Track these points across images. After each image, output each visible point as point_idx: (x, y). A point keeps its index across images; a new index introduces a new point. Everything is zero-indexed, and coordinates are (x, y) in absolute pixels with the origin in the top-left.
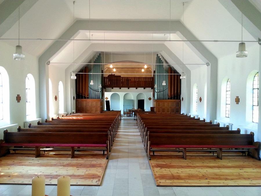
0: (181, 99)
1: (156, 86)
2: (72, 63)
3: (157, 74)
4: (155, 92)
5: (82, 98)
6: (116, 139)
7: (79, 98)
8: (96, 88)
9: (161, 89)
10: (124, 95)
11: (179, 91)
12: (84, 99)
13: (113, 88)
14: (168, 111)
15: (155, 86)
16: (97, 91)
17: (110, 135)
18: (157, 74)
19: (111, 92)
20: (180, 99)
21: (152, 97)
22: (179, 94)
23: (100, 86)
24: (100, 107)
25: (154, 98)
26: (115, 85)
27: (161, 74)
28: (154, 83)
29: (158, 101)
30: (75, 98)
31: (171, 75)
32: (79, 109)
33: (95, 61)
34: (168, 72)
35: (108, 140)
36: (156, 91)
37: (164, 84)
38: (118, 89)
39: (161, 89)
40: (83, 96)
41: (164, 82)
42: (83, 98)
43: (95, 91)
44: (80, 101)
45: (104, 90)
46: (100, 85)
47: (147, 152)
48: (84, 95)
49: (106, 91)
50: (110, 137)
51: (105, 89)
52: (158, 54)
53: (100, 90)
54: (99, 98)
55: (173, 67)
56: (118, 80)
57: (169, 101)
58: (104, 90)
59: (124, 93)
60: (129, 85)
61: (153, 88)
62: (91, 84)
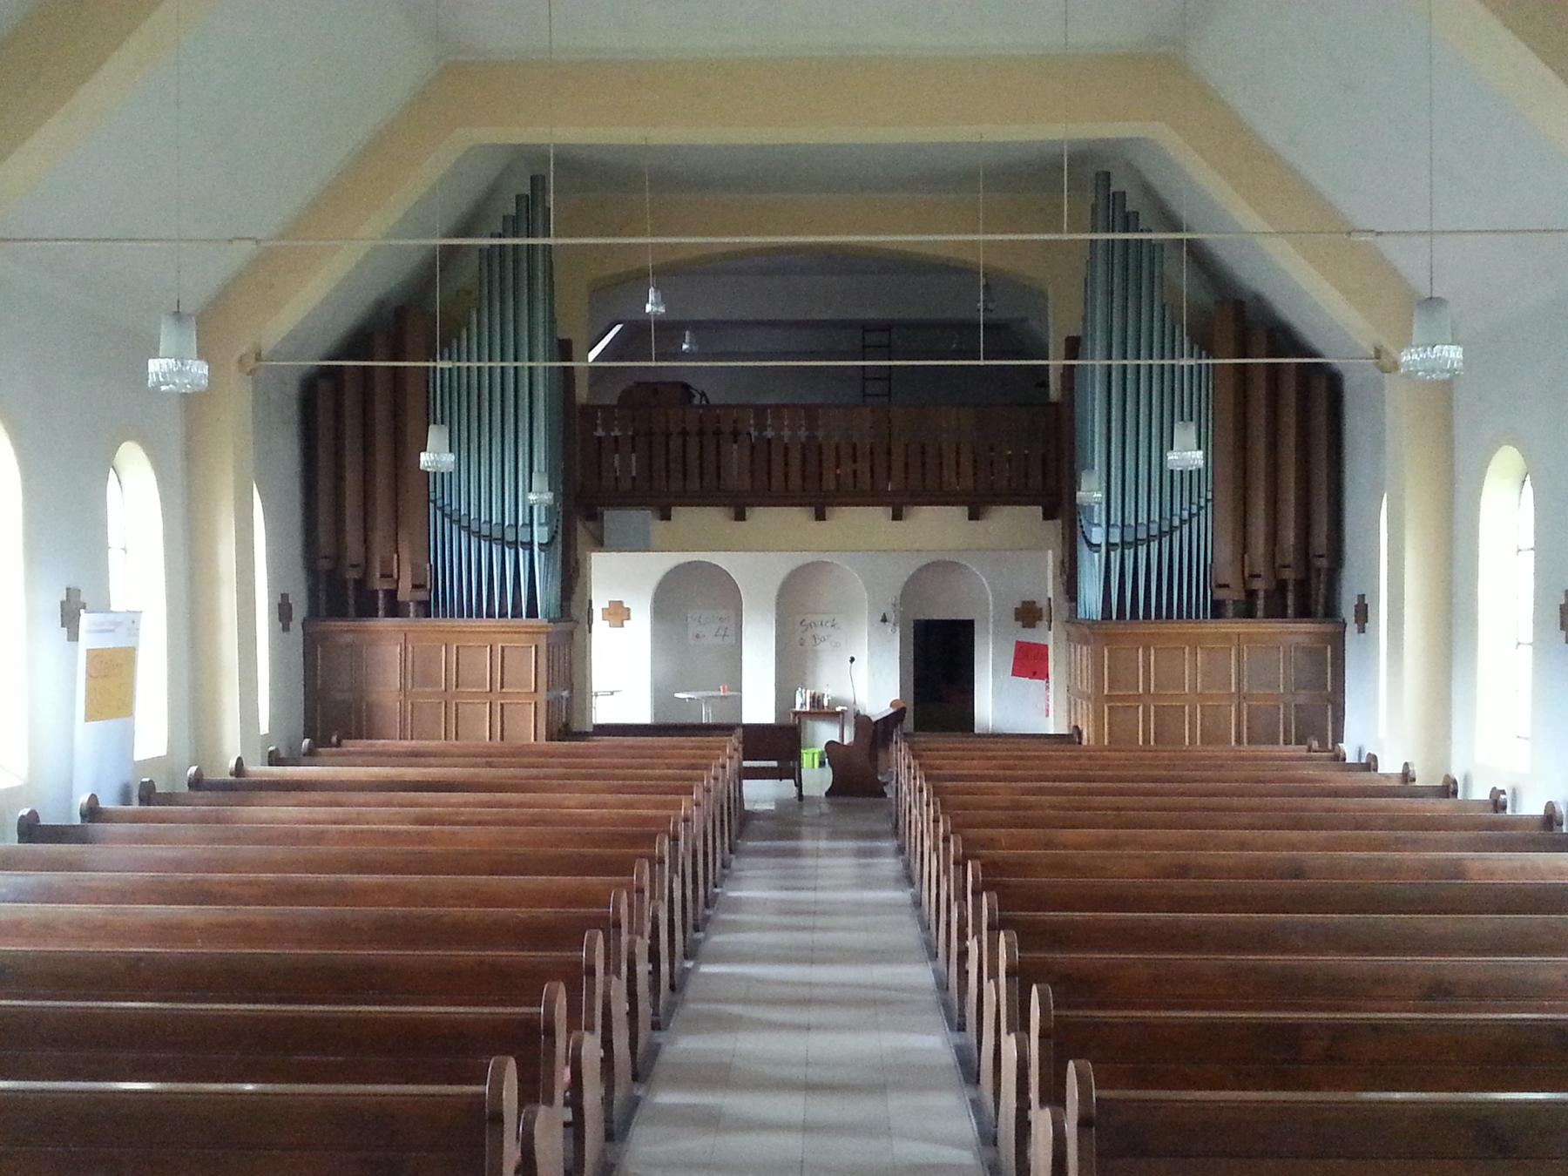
0: (1348, 612)
1: (1090, 492)
2: (282, 237)
3: (1100, 362)
4: (1083, 551)
5: (367, 610)
6: (706, 969)
7: (338, 612)
8: (489, 510)
9: (1143, 518)
10: (778, 581)
11: (1320, 540)
12: (383, 624)
13: (666, 517)
14: (1212, 736)
15: (1083, 487)
16: (515, 544)
18: (1100, 362)
19: (647, 548)
20: (1331, 612)
21: (1049, 588)
22: (1323, 563)
23: (540, 495)
24: (542, 697)
25: (1074, 611)
26: (694, 484)
27: (1131, 362)
28: (1072, 462)
29: (1111, 639)
30: (299, 611)
31: (1109, 366)
32: (329, 711)
33: (511, 210)
34: (1204, 343)
35: (590, 1028)
36: (1097, 536)
37: (1187, 455)
38: (713, 518)
39: (1143, 518)
40: (345, 581)
41: (1186, 434)
42: (373, 613)
43: (490, 539)
44: (349, 638)
45: (582, 532)
46: (540, 481)
47: (809, 1028)
48: (380, 585)
49: (600, 544)
50: (632, 944)
51: (590, 524)
52: (1108, 175)
53: (540, 535)
54: (532, 613)
55: (1258, 298)
56: (684, 433)
57: (1227, 637)
58: (582, 532)
59: (779, 565)
60: (830, 483)
61: (1058, 503)
62: (426, 459)
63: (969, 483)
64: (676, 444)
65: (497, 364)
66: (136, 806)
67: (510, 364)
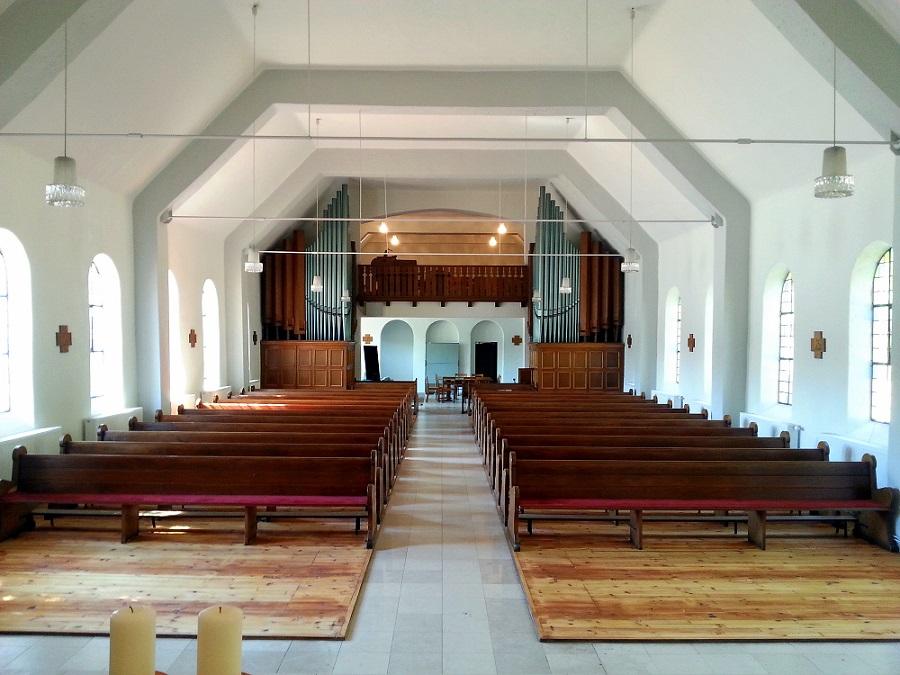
0: (625, 341)
1: (537, 297)
3: (541, 255)
4: (535, 318)
5: (283, 337)
7: (273, 338)
8: (330, 303)
9: (555, 307)
10: (427, 327)
11: (617, 315)
12: (290, 342)
13: (388, 305)
14: (579, 383)
16: (336, 314)
17: (380, 465)
18: (541, 255)
19: (381, 315)
20: (620, 340)
21: (523, 335)
22: (617, 324)
23: (346, 297)
24: (345, 369)
25: (532, 339)
26: (398, 293)
27: (556, 255)
28: (532, 286)
29: (544, 349)
30: (259, 338)
31: (590, 258)
32: (272, 376)
34: (578, 248)
35: (373, 483)
36: (540, 313)
37: (566, 288)
38: (406, 306)
39: (555, 307)
41: (566, 282)
42: (285, 339)
44: (275, 348)
45: (359, 309)
46: (346, 293)
48: (289, 329)
49: (365, 314)
51: (361, 308)
52: (544, 187)
53: (345, 311)
54: (342, 338)
55: (596, 231)
56: (407, 275)
57: (584, 349)
58: (359, 309)
59: (428, 322)
60: (447, 293)
61: (526, 301)
62: (313, 288)
63: (495, 294)
64: (392, 277)
65: (556, 255)
66: (363, 344)
67: (551, 255)
